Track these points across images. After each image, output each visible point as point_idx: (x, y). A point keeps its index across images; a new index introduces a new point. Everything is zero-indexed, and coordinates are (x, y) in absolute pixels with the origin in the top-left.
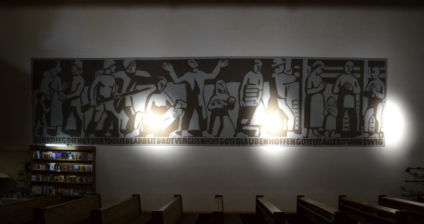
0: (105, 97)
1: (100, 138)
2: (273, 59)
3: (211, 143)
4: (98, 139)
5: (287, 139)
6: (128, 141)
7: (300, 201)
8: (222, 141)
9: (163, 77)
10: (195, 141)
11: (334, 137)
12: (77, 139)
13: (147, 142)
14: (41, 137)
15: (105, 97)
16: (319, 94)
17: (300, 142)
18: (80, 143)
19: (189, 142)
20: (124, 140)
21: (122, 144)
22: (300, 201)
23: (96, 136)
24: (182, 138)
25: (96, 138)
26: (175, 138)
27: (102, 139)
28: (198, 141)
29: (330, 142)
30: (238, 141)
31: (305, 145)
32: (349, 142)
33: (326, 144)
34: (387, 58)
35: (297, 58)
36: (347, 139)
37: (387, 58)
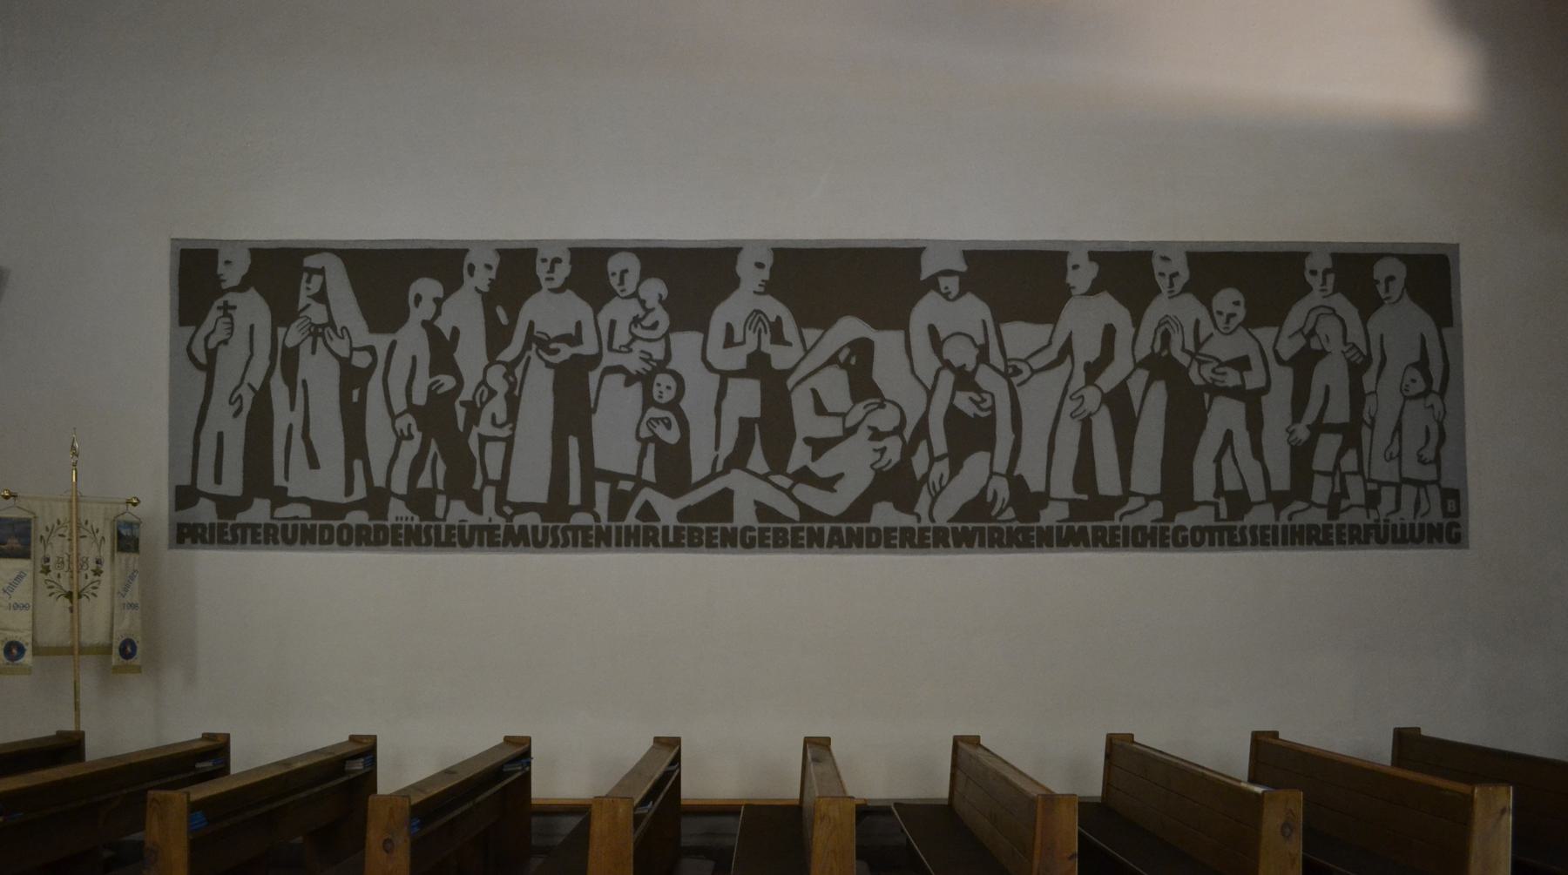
0: (1092, 362)
1: (689, 528)
2: (466, 251)
3: (849, 546)
4: (715, 529)
5: (1261, 527)
6: (781, 538)
7: (964, 748)
8: (1456, 534)
9: (407, 297)
10: (1256, 536)
11: (402, 519)
12: (805, 531)
13: (787, 540)
14: (227, 524)
15: (1092, 362)
16: (827, 368)
17: (1185, 538)
18: (1045, 547)
19: (748, 541)
20: (1167, 533)
21: (580, 548)
22: (964, 748)
23: (543, 520)
24: (1269, 526)
25: (371, 524)
26: (1404, 522)
27: (699, 530)
28: (1245, 536)
29: (249, 532)
30: (749, 534)
31: (1203, 546)
32: (540, 538)
33: (840, 547)
34: (1458, 245)
35: (800, 246)
36: (436, 526)
37: (1458, 245)
